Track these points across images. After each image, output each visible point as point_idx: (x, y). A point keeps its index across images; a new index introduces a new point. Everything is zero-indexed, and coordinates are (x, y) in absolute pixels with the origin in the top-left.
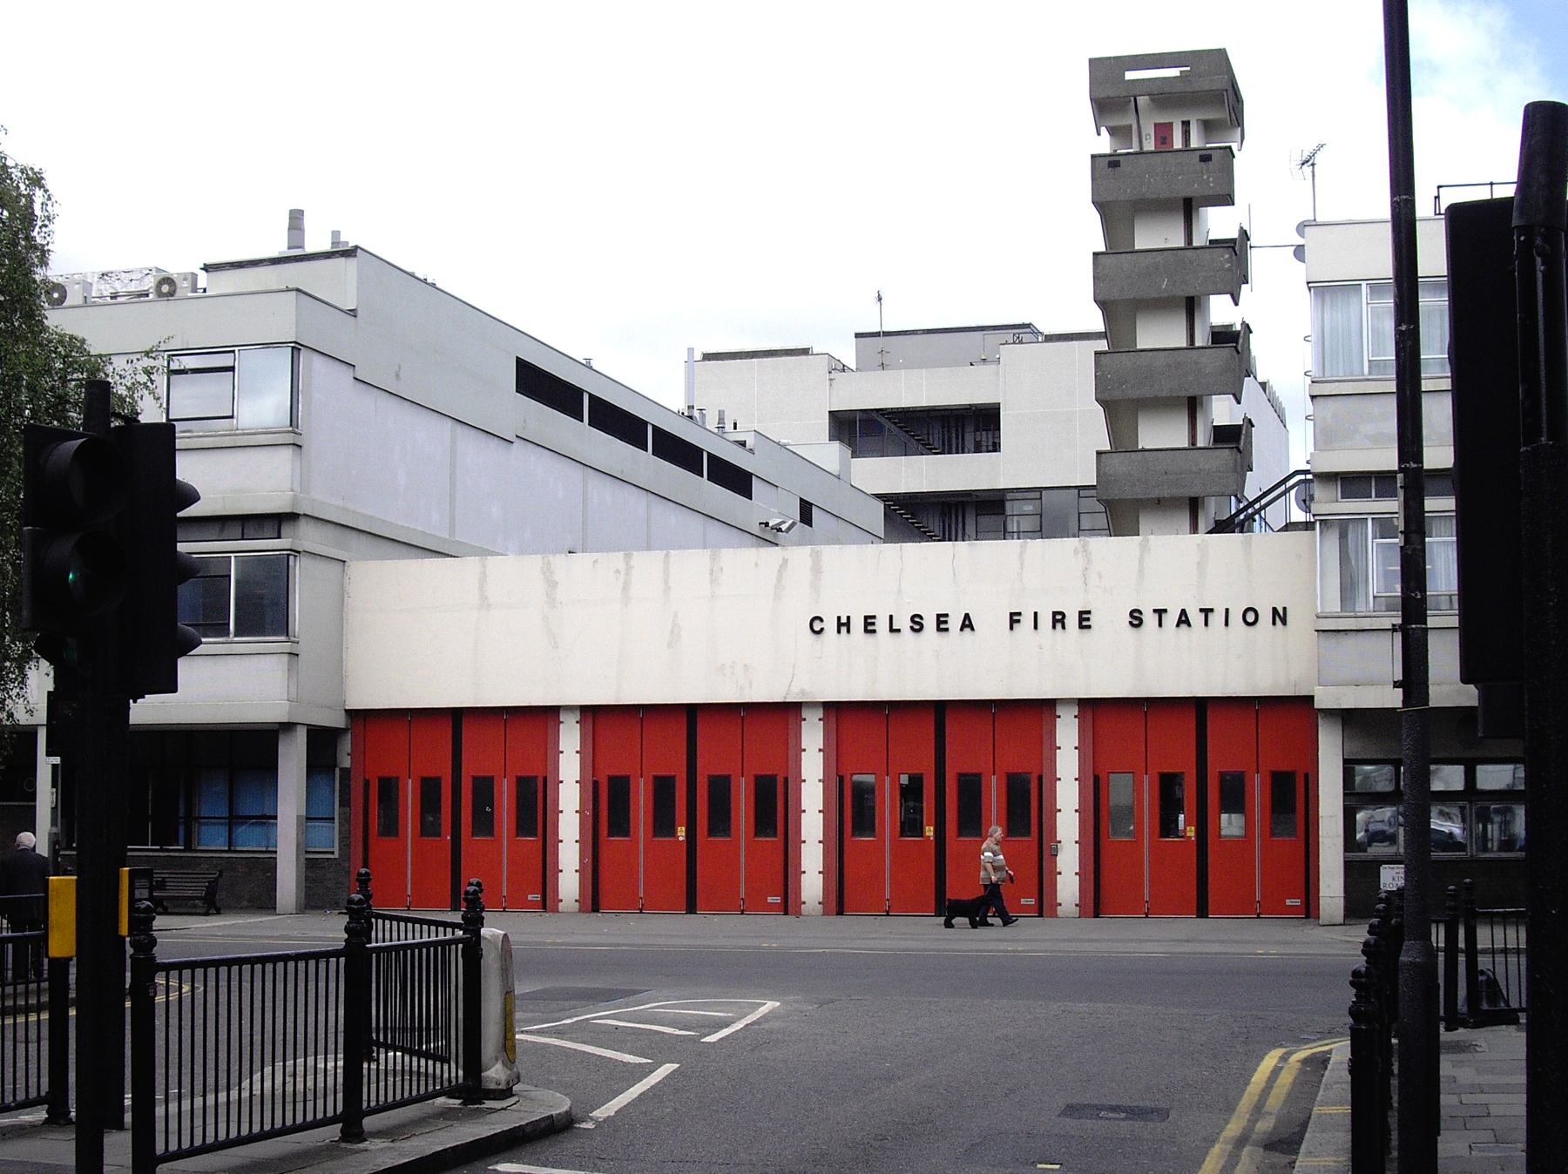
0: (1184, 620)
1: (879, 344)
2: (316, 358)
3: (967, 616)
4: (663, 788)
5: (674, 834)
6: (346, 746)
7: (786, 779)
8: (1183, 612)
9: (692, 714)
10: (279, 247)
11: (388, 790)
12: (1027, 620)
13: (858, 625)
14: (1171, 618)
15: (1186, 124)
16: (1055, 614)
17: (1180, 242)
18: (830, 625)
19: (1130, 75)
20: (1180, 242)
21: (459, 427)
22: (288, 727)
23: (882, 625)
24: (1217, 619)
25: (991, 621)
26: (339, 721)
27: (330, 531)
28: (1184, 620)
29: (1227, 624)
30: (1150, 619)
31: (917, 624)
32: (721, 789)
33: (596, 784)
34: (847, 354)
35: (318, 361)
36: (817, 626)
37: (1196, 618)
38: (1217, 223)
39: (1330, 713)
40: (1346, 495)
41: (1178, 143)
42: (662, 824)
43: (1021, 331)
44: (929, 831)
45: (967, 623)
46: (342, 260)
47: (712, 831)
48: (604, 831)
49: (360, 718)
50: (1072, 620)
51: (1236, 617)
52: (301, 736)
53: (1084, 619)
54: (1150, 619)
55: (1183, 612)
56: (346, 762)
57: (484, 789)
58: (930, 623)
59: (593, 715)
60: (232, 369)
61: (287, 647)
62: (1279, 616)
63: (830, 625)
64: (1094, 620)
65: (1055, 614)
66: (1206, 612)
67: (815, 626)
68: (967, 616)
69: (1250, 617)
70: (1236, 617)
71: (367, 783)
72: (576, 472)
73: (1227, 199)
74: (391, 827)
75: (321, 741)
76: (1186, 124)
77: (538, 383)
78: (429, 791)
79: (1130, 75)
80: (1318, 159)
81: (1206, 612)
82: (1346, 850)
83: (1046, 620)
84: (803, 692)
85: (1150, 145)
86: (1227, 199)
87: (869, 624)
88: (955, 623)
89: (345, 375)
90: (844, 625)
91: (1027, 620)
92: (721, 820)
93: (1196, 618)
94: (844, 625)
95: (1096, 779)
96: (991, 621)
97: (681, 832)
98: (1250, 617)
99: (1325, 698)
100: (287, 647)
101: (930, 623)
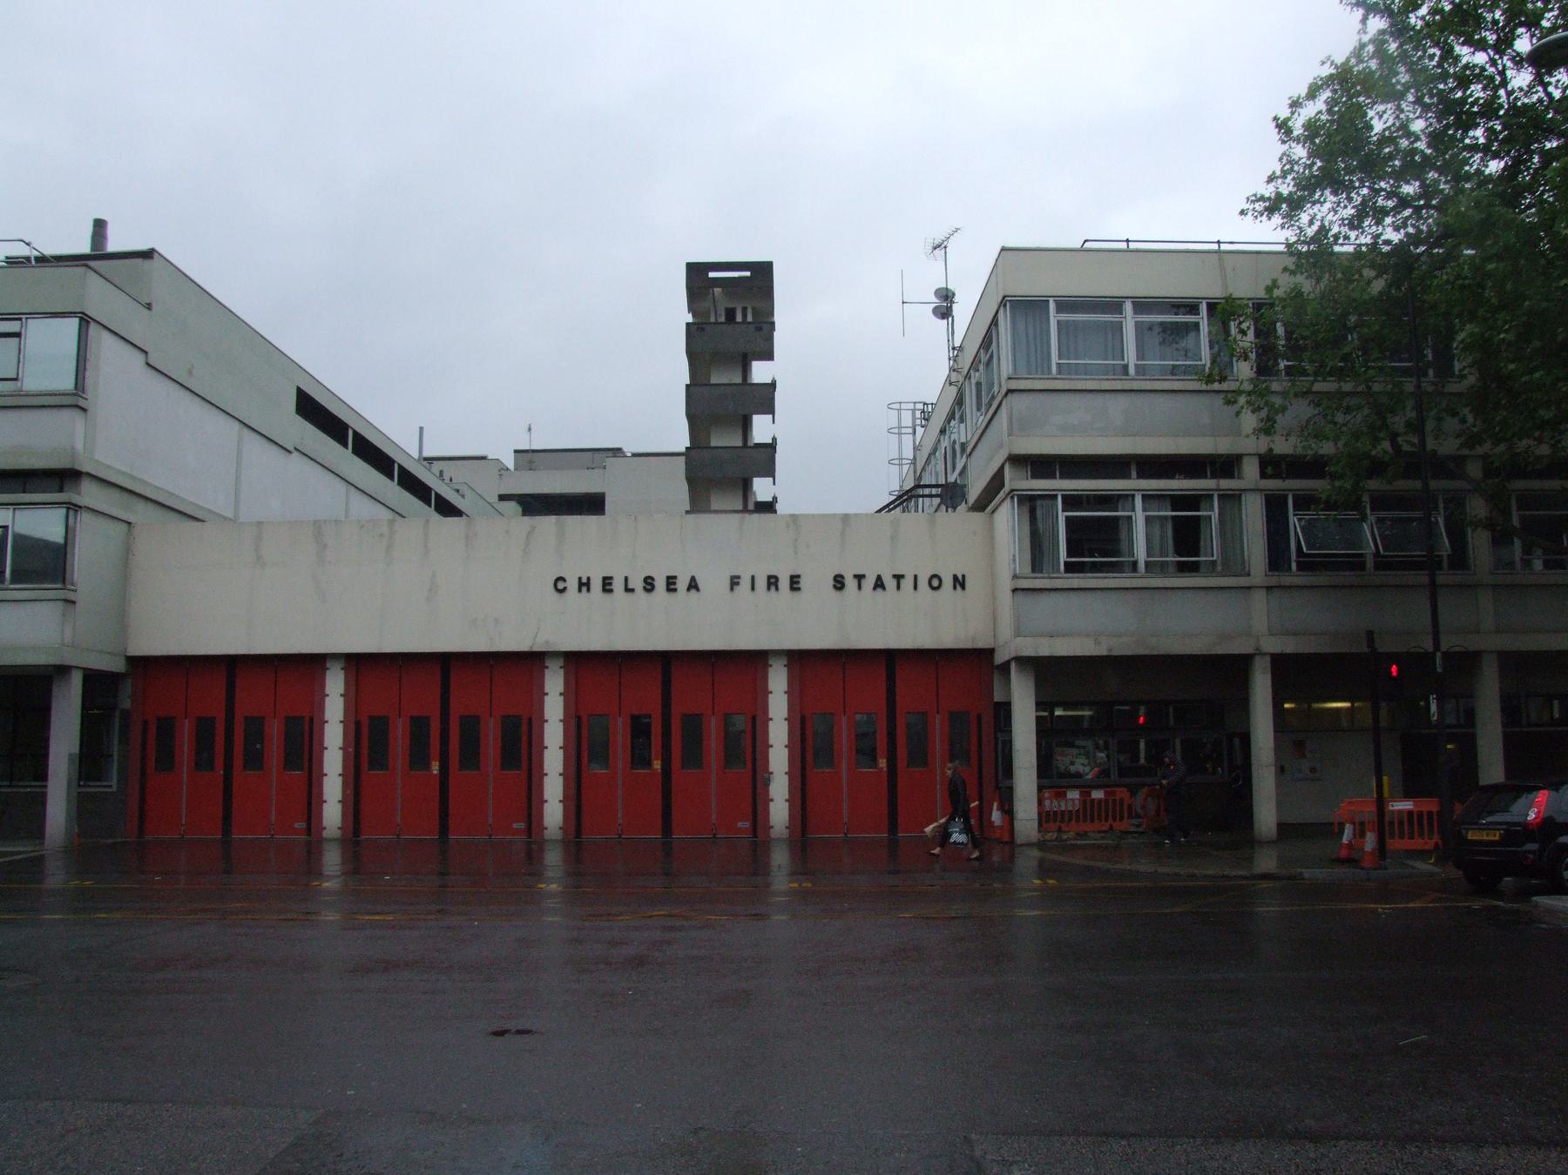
0: (879, 584)
1: (527, 458)
2: (106, 335)
3: (693, 579)
4: (419, 726)
5: (428, 767)
6: (127, 689)
7: (530, 719)
8: (879, 578)
9: (446, 663)
10: (85, 248)
11: (166, 729)
12: (745, 582)
13: (596, 585)
14: (869, 582)
15: (744, 310)
16: (769, 577)
17: (739, 380)
18: (572, 584)
19: (712, 275)
20: (739, 380)
21: (246, 431)
22: (63, 670)
23: (618, 585)
24: (907, 583)
25: (714, 583)
26: (118, 666)
27: (115, 495)
28: (879, 584)
29: (915, 588)
30: (851, 583)
31: (649, 585)
32: (471, 727)
33: (358, 724)
34: (509, 462)
35: (107, 338)
36: (561, 585)
37: (890, 583)
38: (760, 372)
39: (1025, 662)
40: (1034, 476)
41: (739, 318)
42: (418, 758)
43: (617, 452)
44: (657, 765)
45: (693, 585)
46: (139, 261)
47: (462, 765)
48: (365, 766)
49: (143, 666)
50: (784, 583)
51: (923, 583)
52: (77, 680)
53: (795, 583)
54: (851, 583)
55: (879, 578)
56: (126, 704)
57: (256, 727)
58: (660, 584)
59: (357, 663)
60: (18, 335)
61: (61, 594)
62: (960, 582)
63: (572, 584)
64: (803, 583)
65: (769, 577)
66: (898, 578)
67: (559, 585)
68: (693, 579)
69: (935, 583)
70: (923, 583)
71: (145, 722)
72: (341, 487)
73: (768, 355)
74: (167, 758)
75: (96, 682)
76: (744, 310)
77: (311, 409)
78: (204, 728)
79: (712, 275)
80: (951, 245)
81: (898, 578)
82: (1039, 776)
83: (761, 583)
84: (547, 642)
85: (722, 319)
86: (768, 355)
87: (607, 584)
88: (682, 584)
89: (140, 358)
90: (584, 585)
91: (745, 582)
92: (471, 754)
93: (890, 583)
94: (584, 585)
95: (803, 719)
96: (714, 583)
97: (435, 768)
98: (935, 583)
99: (1010, 645)
100: (61, 594)
101: (660, 584)
